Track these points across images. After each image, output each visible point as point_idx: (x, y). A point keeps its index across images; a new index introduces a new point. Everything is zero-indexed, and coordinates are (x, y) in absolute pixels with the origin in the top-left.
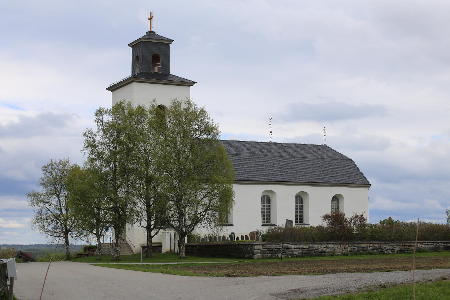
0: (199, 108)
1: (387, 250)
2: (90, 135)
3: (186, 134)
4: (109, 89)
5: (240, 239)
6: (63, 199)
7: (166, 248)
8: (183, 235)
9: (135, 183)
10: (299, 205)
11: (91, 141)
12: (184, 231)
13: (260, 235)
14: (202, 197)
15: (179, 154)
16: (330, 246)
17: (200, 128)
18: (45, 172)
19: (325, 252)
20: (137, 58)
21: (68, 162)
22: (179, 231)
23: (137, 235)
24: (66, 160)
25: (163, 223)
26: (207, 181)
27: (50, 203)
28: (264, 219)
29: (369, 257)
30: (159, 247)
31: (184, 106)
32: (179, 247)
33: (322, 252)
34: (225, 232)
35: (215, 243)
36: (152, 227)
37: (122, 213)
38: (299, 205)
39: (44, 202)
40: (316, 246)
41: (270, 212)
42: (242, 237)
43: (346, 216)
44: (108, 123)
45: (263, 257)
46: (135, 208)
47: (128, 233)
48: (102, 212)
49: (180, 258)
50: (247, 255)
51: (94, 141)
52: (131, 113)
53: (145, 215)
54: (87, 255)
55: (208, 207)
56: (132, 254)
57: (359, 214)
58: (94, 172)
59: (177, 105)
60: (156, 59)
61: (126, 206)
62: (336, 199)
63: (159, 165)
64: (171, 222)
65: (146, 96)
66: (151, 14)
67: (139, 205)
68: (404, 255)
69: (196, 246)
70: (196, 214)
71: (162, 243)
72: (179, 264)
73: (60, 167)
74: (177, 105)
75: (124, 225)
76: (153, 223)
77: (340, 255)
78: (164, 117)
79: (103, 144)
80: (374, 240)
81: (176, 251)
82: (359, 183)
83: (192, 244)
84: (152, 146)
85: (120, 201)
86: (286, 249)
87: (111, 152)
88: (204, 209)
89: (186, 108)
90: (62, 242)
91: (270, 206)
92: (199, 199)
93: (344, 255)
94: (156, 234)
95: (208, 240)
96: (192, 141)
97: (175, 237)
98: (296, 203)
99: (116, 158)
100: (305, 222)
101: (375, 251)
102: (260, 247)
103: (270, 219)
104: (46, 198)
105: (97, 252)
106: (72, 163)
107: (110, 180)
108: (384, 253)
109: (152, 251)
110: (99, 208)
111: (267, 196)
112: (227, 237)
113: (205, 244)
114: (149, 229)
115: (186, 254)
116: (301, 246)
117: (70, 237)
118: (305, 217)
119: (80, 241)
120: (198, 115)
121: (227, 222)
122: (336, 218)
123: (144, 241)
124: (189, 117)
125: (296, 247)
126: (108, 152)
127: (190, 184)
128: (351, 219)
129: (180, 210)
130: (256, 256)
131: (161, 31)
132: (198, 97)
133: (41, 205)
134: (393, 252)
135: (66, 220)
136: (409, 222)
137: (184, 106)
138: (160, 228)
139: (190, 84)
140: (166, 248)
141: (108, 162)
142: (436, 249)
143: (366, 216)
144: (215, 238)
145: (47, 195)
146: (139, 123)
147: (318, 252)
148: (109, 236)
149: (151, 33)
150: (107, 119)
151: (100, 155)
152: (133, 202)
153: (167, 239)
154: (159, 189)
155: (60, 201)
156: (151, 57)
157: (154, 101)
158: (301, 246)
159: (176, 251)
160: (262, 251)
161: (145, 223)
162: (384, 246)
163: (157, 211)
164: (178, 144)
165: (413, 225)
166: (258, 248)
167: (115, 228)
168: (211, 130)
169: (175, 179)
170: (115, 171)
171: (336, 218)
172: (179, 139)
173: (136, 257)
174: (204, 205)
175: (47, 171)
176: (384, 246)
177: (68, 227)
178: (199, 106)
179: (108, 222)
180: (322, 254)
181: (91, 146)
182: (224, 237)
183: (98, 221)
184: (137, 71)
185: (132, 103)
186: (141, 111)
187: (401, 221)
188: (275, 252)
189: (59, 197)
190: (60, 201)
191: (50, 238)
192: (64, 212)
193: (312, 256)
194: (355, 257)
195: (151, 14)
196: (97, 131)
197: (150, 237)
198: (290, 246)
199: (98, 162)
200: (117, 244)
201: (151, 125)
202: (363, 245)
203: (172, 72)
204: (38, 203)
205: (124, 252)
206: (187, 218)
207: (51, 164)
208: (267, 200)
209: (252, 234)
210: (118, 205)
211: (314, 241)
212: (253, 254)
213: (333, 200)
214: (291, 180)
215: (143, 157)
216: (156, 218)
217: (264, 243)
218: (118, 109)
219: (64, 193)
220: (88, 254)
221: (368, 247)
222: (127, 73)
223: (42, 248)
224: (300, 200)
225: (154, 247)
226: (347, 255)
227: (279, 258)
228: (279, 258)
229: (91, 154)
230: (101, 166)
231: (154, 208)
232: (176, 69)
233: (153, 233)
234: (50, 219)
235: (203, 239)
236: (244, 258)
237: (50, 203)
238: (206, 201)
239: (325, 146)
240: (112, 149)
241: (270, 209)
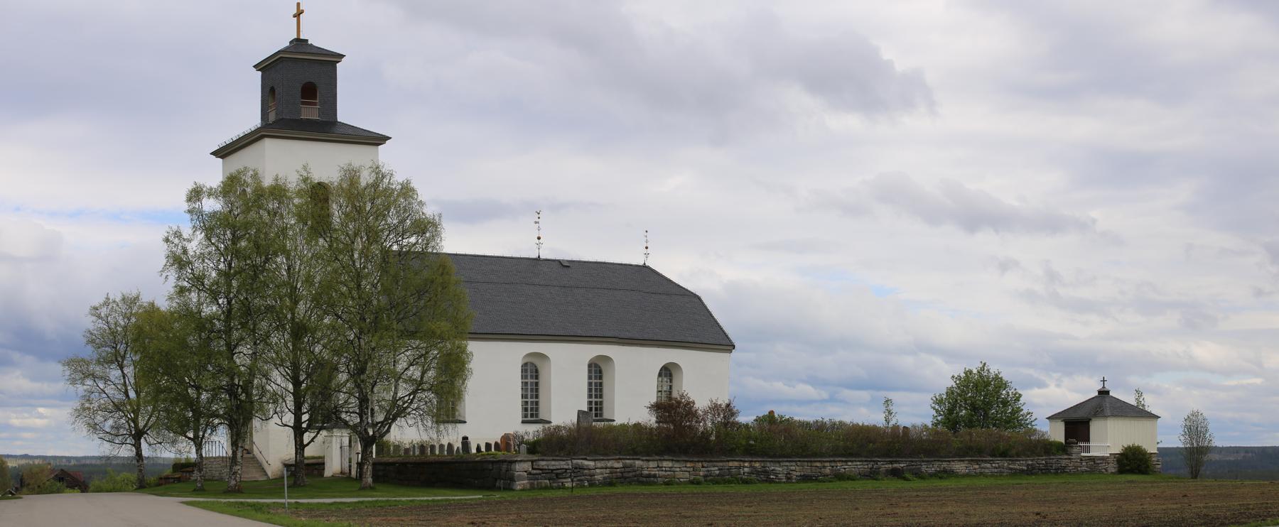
0: (400, 181)
1: (776, 474)
2: (176, 241)
3: (373, 236)
4: (215, 153)
5: (483, 449)
6: (129, 371)
7: (334, 466)
8: (367, 442)
9: (268, 337)
10: (593, 381)
11: (179, 251)
12: (371, 433)
13: (522, 442)
14: (405, 365)
15: (358, 276)
16: (665, 464)
17: (402, 221)
18: (94, 318)
19: (655, 476)
20: (272, 90)
21: (137, 298)
22: (359, 434)
23: (274, 441)
24: (134, 294)
25: (327, 418)
26: (412, 335)
27: (106, 380)
28: (526, 410)
29: (744, 489)
30: (318, 466)
31: (366, 178)
32: (360, 465)
33: (649, 476)
34: (451, 436)
35: (432, 458)
36: (304, 426)
37: (243, 397)
38: (593, 381)
39: (94, 377)
40: (638, 463)
41: (537, 397)
42: (488, 446)
43: (697, 406)
44: (214, 215)
45: (532, 484)
46: (268, 388)
47: (256, 438)
48: (204, 396)
49: (363, 489)
50: (500, 483)
51: (185, 251)
52: (260, 193)
53: (290, 400)
54: (179, 480)
55: (418, 386)
56: (265, 478)
57: (723, 401)
58: (189, 316)
59: (352, 177)
60: (309, 92)
61: (251, 382)
62: (668, 372)
63: (316, 300)
64: (343, 416)
65: (289, 163)
66: (298, 4)
67: (279, 381)
68: (811, 486)
69: (393, 464)
70: (395, 400)
71: (323, 458)
72: (362, 502)
73: (124, 308)
74: (352, 177)
75: (248, 419)
76: (305, 417)
77: (685, 483)
78: (326, 200)
79: (202, 257)
80: (751, 455)
81: (354, 473)
82: (712, 341)
83: (386, 459)
84: (301, 258)
85: (240, 375)
86: (578, 469)
87: (220, 272)
88: (411, 389)
89: (371, 181)
90: (126, 452)
91: (537, 384)
92: (400, 368)
93: (692, 482)
94: (312, 440)
95: (417, 453)
96: (386, 252)
97: (350, 446)
98: (590, 378)
99: (230, 285)
100: (606, 416)
101: (753, 476)
102: (527, 466)
103: (537, 409)
104: (98, 370)
105: (196, 475)
106: (145, 299)
107: (219, 331)
108: (771, 481)
109: (304, 472)
110: (198, 388)
111: (532, 364)
112: (458, 444)
113: (411, 460)
114: (298, 431)
115: (374, 481)
116: (609, 464)
117: (144, 445)
118: (605, 405)
119: (166, 451)
120: (398, 196)
121: (454, 415)
122: (672, 409)
123: (289, 453)
124: (378, 203)
125: (599, 464)
126: (214, 274)
127: (381, 338)
128: (706, 413)
129: (361, 392)
130: (519, 485)
131: (319, 38)
132: (395, 162)
133: (89, 382)
134: (789, 478)
135: (136, 412)
136: (811, 419)
137: (366, 178)
138: (320, 429)
139: (377, 140)
140: (334, 466)
141: (214, 296)
142: (872, 475)
143: (736, 406)
144: (433, 447)
145: (99, 362)
146: (275, 214)
147: (641, 475)
148: (219, 444)
149: (299, 43)
150: (211, 205)
151: (198, 280)
152: (266, 376)
153: (334, 450)
154: (317, 349)
155: (124, 376)
156: (300, 88)
157: (305, 168)
158: (609, 464)
159: (354, 473)
160: (530, 474)
161: (289, 418)
162: (771, 467)
163: (313, 393)
164: (356, 256)
165: (820, 427)
166: (522, 468)
167: (231, 427)
168: (425, 227)
169: (351, 328)
170: (229, 311)
171: (672, 409)
172: (359, 245)
173: (272, 486)
174: (410, 380)
175: (99, 317)
176: (771, 467)
177: (141, 424)
178: (399, 179)
179: (217, 416)
180: (648, 480)
181: (179, 261)
182: (450, 445)
183: (198, 414)
184: (272, 117)
185: (260, 172)
186: (278, 192)
187: (796, 418)
188: (557, 475)
189: (122, 368)
190: (124, 376)
191: (107, 445)
192: (132, 394)
193: (630, 483)
194: (718, 489)
195: (298, 4)
196: (191, 232)
197: (300, 446)
198: (586, 463)
199: (194, 296)
200: (233, 459)
201: (301, 219)
202: (731, 464)
203: (342, 116)
204: (82, 380)
205: (251, 475)
206: (376, 408)
207: (106, 303)
208: (532, 373)
209: (506, 438)
210: (236, 381)
211: (635, 453)
212: (512, 479)
213: (660, 375)
214: (579, 332)
215: (284, 284)
216: (312, 409)
217: (535, 458)
218: (231, 186)
219: (131, 357)
220: (181, 479)
221: (739, 468)
222: (252, 120)
223: (98, 462)
224: (597, 370)
225: (308, 465)
226: (699, 483)
227: (563, 487)
228: (563, 487)
229: (179, 278)
230: (200, 304)
231: (308, 388)
232: (347, 113)
233: (307, 437)
234: (106, 410)
235: (407, 451)
236: (492, 487)
237: (106, 380)
238: (415, 372)
239: (644, 266)
240: (222, 266)
241: (537, 390)
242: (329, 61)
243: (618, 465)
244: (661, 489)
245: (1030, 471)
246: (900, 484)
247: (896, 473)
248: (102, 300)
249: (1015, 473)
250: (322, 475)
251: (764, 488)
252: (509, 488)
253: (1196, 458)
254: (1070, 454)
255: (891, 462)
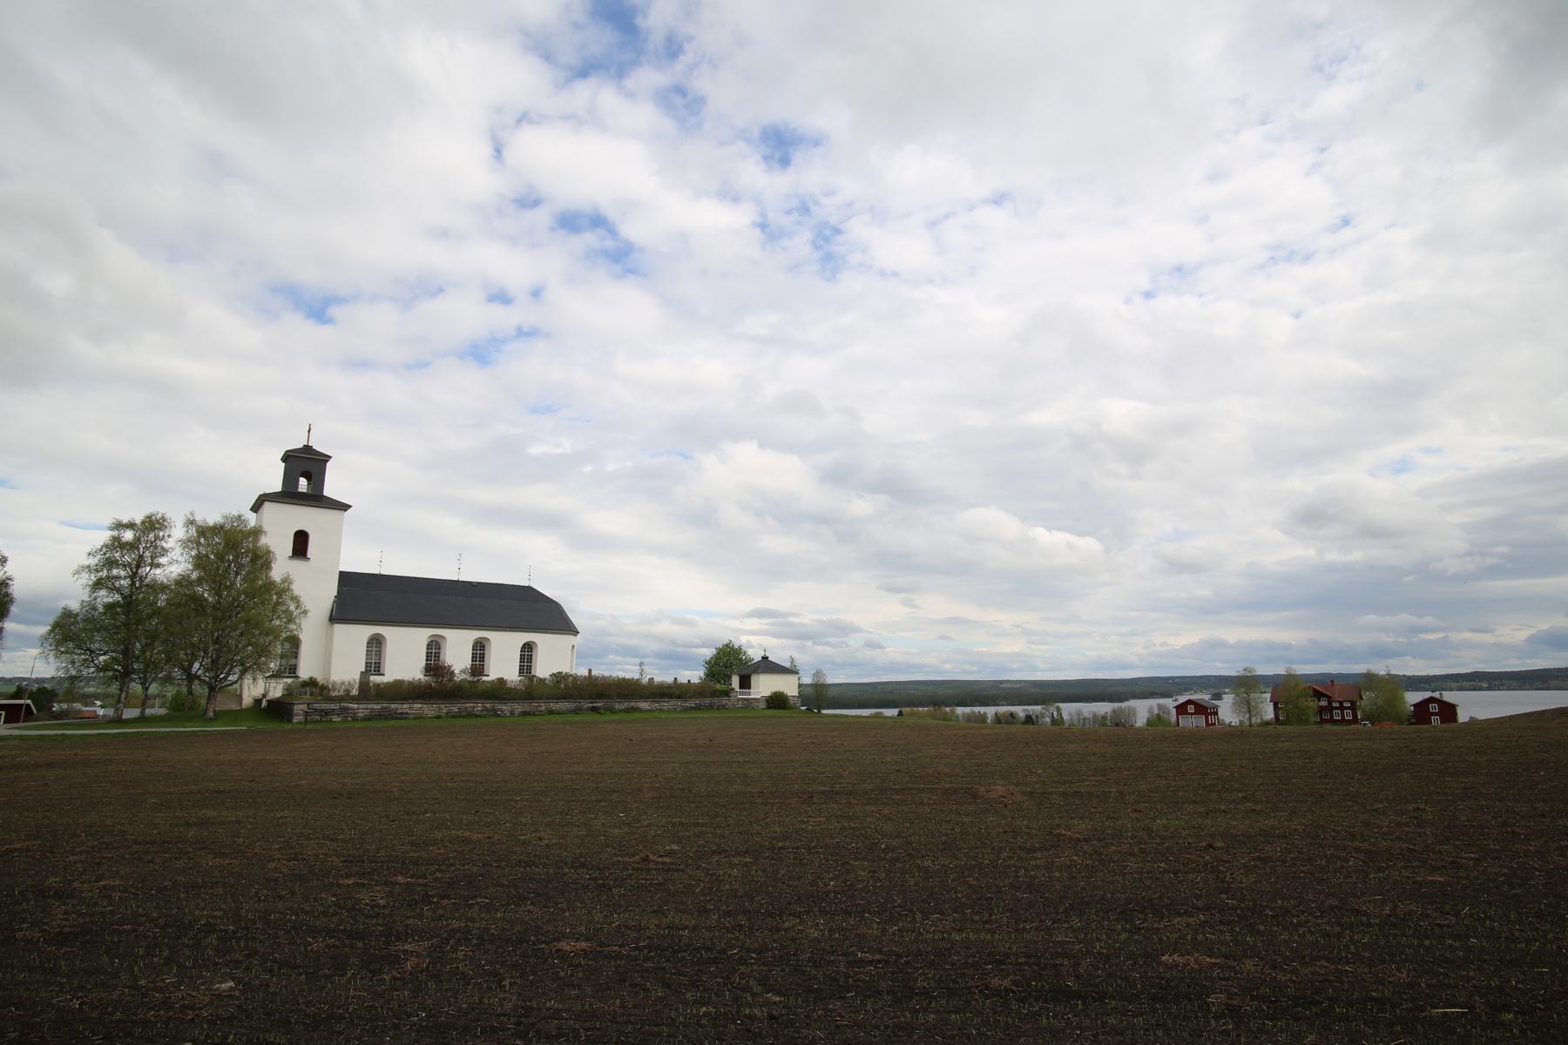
59: (186, 543)
131: (318, 446)
142: (577, 711)
211: (393, 699)
224: (376, 643)
244: (412, 723)
245: (698, 708)
246: (597, 717)
247: (594, 709)
248: (758, 231)
249: (686, 709)
250: (1455, 720)
251: (493, 720)
252: (290, 721)
253: (818, 696)
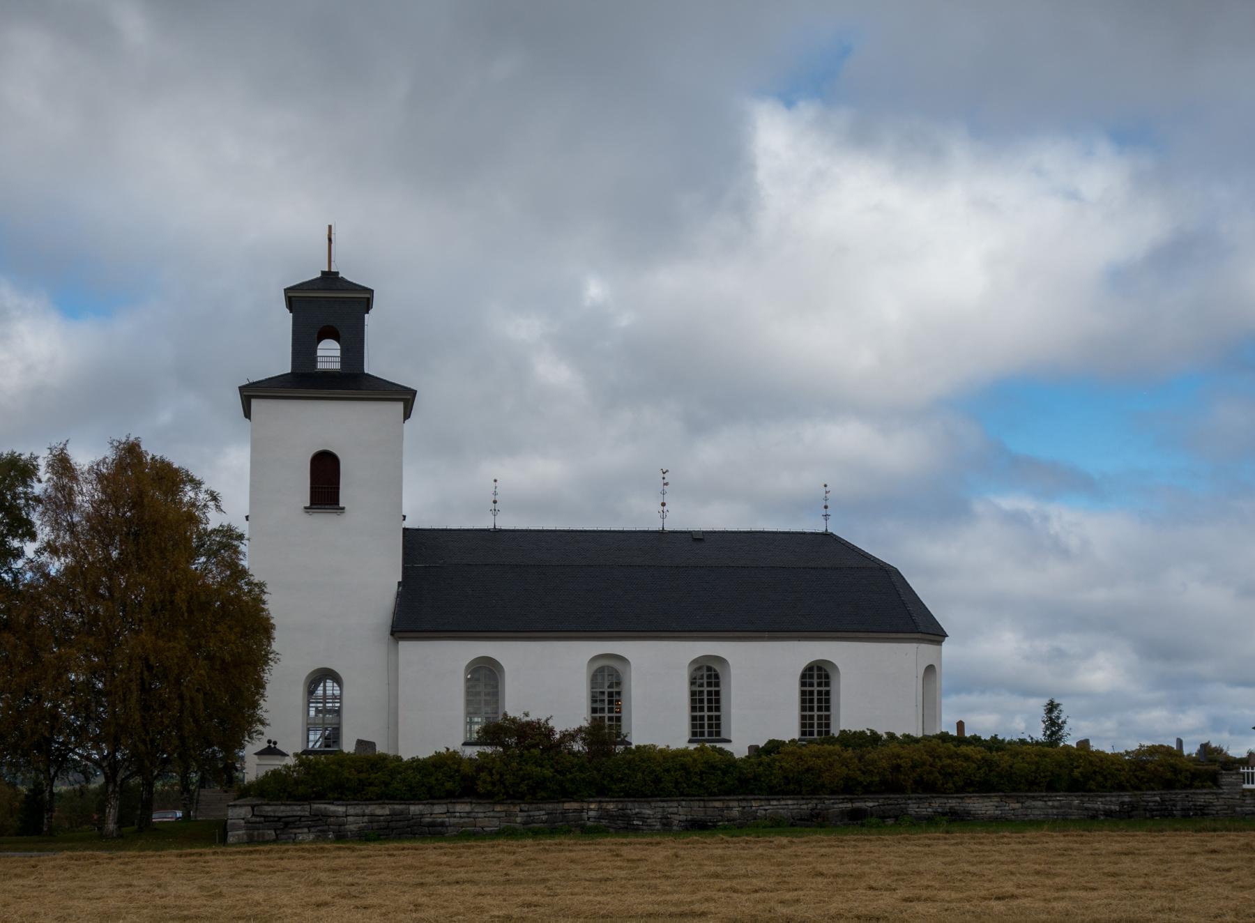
1: (643, 819)
16: (459, 808)
19: (442, 824)
33: (432, 825)
40: (415, 809)
62: (485, 677)
101: (604, 822)
116: (368, 810)
125: (351, 810)
147: (420, 824)
198: (332, 808)
202: (567, 806)
221: (582, 810)
242: (362, 300)
243: (386, 811)
254: (1219, 787)
255: (851, 800)
